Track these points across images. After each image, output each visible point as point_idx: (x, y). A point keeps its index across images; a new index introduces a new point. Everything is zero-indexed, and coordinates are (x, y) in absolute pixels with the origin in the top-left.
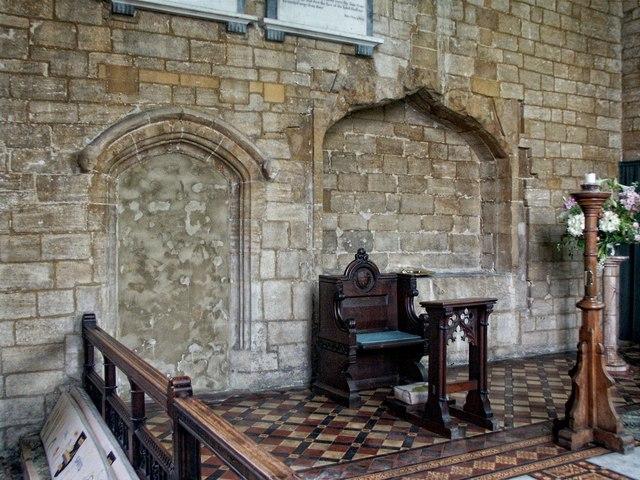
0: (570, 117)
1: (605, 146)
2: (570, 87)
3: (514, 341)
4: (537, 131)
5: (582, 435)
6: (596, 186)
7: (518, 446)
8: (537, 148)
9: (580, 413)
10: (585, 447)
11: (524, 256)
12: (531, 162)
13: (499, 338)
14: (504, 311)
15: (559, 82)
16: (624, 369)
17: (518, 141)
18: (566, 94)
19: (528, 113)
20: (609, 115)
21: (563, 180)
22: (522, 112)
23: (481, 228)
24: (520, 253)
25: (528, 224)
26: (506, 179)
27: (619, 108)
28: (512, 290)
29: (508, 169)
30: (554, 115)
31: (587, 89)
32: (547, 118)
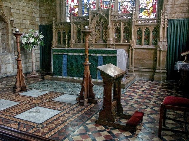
0: (25, 13)
1: (35, 21)
2: (25, 5)
3: (12, 71)
4: (15, 16)
5: (19, 89)
6: (19, 32)
7: (71, 108)
8: (16, 21)
9: (18, 84)
10: (19, 91)
11: (13, 49)
12: (14, 24)
13: (7, 71)
14: (8, 64)
15: (21, 3)
16: (37, 75)
17: (10, 19)
18: (24, 6)
19: (12, 11)
20: (36, 13)
21: (24, 29)
22: (11, 10)
23: (2, 42)
24: (12, 49)
25: (14, 41)
26: (7, 28)
27: (38, 11)
28: (10, 58)
29: (7, 26)
30: (21, 12)
31: (29, 6)
32: (18, 13)
